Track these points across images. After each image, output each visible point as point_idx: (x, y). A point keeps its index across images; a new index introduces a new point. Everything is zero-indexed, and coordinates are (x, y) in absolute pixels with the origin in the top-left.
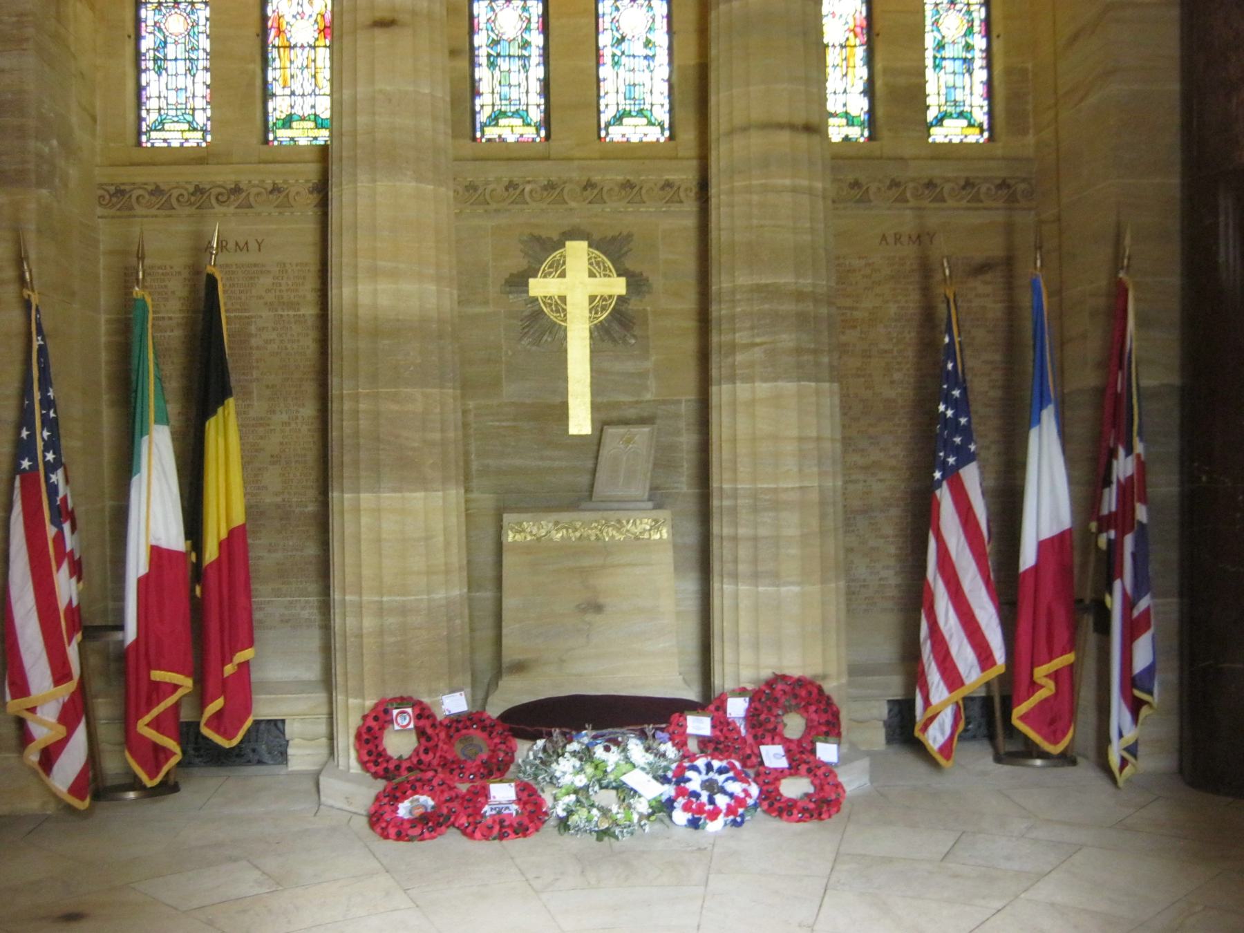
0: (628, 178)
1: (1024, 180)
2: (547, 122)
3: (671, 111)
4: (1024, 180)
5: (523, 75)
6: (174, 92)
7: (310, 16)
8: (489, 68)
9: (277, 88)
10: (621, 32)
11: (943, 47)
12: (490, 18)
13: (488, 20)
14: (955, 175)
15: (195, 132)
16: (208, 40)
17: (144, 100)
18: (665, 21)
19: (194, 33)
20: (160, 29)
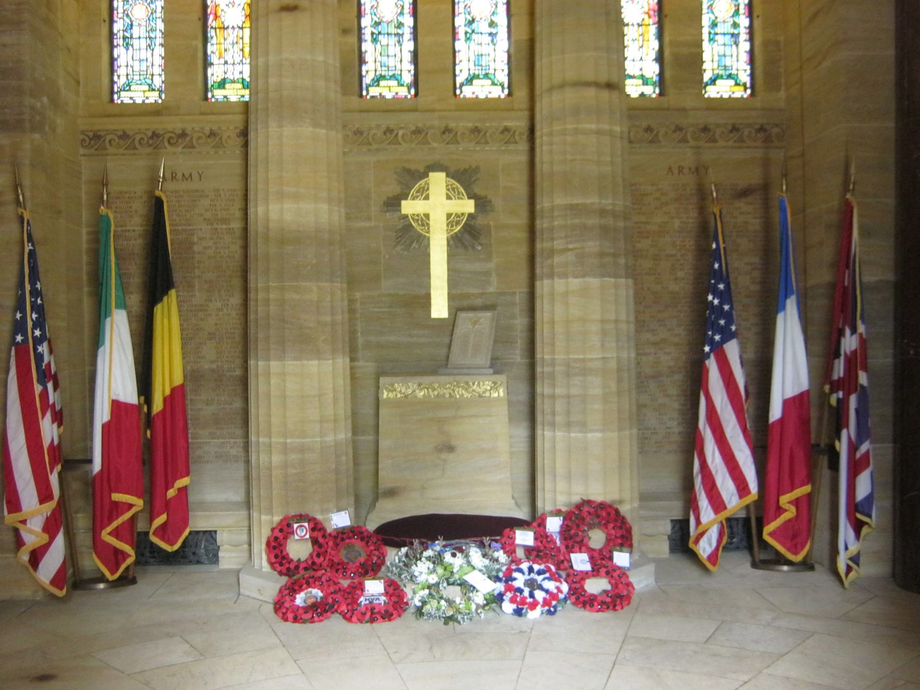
0: (476, 125)
1: (777, 125)
2: (416, 83)
3: (509, 75)
4: (777, 125)
8: (373, 43)
9: (214, 59)
10: (472, 15)
13: (372, 7)
15: (154, 92)
17: (116, 68)
19: (153, 18)
20: (127, 15)
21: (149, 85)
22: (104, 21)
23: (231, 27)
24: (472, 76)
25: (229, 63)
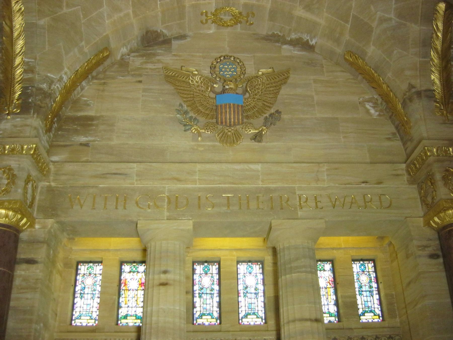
0: (250, 338)
1: (398, 335)
2: (220, 317)
3: (265, 313)
4: (398, 335)
5: (211, 300)
6: (86, 305)
7: (136, 279)
8: (199, 298)
9: (123, 304)
10: (246, 284)
11: (362, 287)
12: (200, 280)
13: (199, 281)
14: (372, 334)
15: (92, 320)
16: (100, 287)
17: (75, 308)
18: (262, 280)
19: (95, 285)
20: (83, 283)
21: (90, 317)
22: (72, 286)
23: (132, 289)
24: (247, 313)
25: (130, 306)
